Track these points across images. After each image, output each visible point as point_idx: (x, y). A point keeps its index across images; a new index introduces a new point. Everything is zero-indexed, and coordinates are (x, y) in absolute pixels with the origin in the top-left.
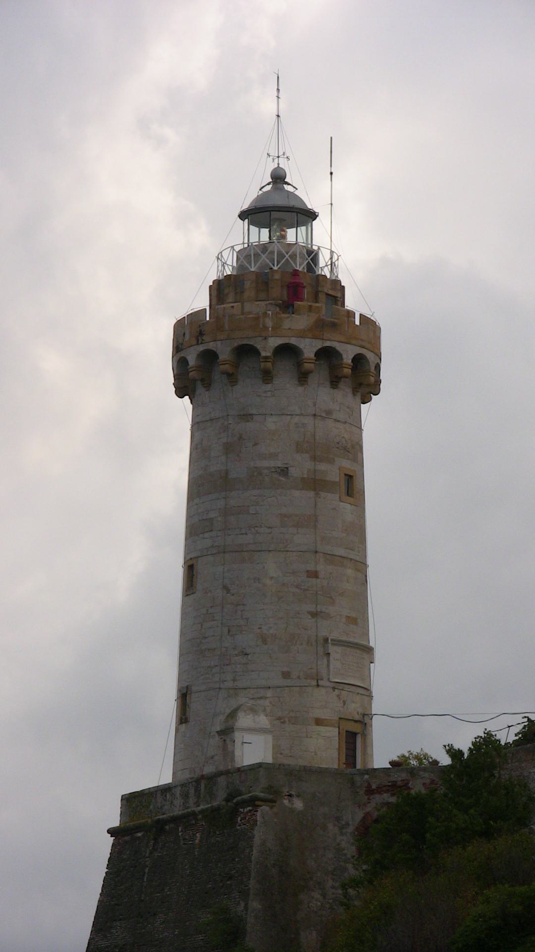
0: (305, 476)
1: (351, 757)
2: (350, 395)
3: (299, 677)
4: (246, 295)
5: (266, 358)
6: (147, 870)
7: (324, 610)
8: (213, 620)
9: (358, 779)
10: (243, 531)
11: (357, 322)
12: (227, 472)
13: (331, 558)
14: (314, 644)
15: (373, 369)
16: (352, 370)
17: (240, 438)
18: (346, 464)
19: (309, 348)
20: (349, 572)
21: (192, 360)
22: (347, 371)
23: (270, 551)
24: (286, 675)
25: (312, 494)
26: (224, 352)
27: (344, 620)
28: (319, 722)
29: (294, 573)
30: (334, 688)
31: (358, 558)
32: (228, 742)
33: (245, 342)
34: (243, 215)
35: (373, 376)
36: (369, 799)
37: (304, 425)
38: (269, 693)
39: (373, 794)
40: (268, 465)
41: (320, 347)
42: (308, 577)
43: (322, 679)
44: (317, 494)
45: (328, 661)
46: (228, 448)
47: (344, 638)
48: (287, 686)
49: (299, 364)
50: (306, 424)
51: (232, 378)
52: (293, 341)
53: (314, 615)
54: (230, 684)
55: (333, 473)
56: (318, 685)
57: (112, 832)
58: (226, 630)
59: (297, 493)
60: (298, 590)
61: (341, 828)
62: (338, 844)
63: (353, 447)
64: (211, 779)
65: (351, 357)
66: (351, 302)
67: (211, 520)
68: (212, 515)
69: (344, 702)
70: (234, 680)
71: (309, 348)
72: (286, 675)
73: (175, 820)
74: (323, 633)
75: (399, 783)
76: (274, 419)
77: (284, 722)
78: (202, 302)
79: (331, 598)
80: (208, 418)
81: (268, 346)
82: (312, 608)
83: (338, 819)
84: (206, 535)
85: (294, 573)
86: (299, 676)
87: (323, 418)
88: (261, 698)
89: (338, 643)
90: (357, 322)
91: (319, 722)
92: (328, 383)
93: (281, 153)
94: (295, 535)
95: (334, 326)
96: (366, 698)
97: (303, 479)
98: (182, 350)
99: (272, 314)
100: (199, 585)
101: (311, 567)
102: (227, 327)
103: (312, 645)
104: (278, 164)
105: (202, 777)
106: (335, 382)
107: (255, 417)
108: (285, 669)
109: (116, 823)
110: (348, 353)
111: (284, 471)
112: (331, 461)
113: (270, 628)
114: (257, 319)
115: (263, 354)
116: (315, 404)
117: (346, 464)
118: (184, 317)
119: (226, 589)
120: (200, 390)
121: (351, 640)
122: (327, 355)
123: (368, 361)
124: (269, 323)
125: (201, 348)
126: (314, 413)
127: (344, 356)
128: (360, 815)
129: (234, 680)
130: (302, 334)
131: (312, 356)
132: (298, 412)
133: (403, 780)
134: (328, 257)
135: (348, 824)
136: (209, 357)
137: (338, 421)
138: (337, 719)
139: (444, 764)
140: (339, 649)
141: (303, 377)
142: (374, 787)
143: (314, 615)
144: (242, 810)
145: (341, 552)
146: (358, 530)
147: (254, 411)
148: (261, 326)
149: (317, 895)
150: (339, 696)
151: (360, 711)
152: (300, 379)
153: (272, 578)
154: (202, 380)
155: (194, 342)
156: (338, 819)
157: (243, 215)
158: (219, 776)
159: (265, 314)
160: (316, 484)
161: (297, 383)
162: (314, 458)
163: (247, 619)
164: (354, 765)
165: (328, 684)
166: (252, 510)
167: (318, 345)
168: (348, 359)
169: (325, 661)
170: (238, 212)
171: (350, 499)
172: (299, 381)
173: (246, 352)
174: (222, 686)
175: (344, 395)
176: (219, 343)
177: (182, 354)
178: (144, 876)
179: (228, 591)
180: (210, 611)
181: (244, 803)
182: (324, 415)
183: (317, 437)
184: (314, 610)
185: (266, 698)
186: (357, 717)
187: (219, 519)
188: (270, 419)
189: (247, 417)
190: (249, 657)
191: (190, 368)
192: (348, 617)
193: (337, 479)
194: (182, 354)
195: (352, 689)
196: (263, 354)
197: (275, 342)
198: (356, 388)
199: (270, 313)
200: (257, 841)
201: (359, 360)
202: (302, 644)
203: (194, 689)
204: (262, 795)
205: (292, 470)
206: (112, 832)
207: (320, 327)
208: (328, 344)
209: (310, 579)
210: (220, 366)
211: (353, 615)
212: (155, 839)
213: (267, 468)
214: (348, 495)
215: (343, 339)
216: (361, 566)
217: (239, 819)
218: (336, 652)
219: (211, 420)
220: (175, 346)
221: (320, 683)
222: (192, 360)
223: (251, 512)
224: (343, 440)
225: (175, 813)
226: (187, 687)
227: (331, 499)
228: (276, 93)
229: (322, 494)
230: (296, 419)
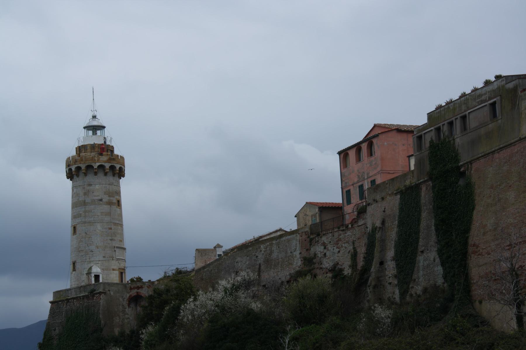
0: (107, 201)
1: (122, 281)
2: (118, 178)
3: (108, 258)
4: (88, 150)
5: (96, 168)
6: (64, 313)
8: (82, 242)
9: (128, 286)
10: (91, 217)
12: (85, 200)
13: (115, 224)
14: (111, 248)
17: (88, 191)
18: (117, 197)
19: (107, 165)
20: (120, 227)
21: (73, 169)
24: (104, 257)
25: (109, 206)
26: (83, 167)
27: (119, 241)
28: (113, 270)
29: (336, 239)
30: (117, 260)
31: (121, 224)
32: (89, 276)
33: (89, 164)
34: (85, 128)
36: (131, 291)
37: (106, 187)
38: (100, 262)
39: (132, 289)
40: (97, 198)
41: (110, 165)
42: (109, 229)
44: (111, 206)
45: (115, 252)
46: (85, 194)
47: (119, 246)
51: (85, 174)
52: (103, 164)
53: (111, 240)
54: (88, 260)
55: (115, 201)
56: (113, 260)
57: (51, 302)
58: (86, 245)
59: (105, 206)
61: (123, 299)
62: (123, 304)
63: (119, 192)
64: (84, 287)
65: (118, 167)
67: (81, 214)
68: (81, 213)
69: (120, 264)
70: (89, 259)
71: (107, 165)
72: (104, 257)
73: (73, 298)
74: (114, 245)
75: (140, 286)
76: (98, 185)
77: (104, 270)
78: (74, 153)
80: (78, 185)
81: (96, 166)
82: (110, 238)
83: (122, 297)
84: (79, 218)
85: (336, 239)
87: (111, 185)
88: (97, 264)
89: (117, 247)
91: (113, 270)
92: (112, 175)
93: (95, 110)
95: (114, 159)
96: (125, 262)
97: (106, 202)
98: (70, 166)
100: (78, 232)
101: (110, 227)
102: (84, 160)
105: (81, 286)
106: (114, 175)
107: (92, 185)
108: (104, 255)
109: (51, 299)
110: (118, 167)
111: (101, 200)
112: (113, 197)
114: (93, 158)
115: (95, 167)
116: (109, 181)
117: (117, 197)
118: (70, 157)
119: (86, 233)
120: (75, 177)
121: (121, 246)
122: (112, 168)
123: (122, 168)
124: (96, 159)
125: (76, 166)
126: (109, 183)
127: (117, 167)
128: (128, 295)
129: (89, 259)
130: (106, 162)
131: (108, 168)
132: (104, 183)
133: (141, 286)
134: (110, 139)
135: (125, 298)
136: (79, 169)
138: (118, 268)
139: (144, 281)
140: (118, 249)
141: (106, 174)
142: (132, 287)
143: (111, 240)
144: (96, 295)
145: (117, 222)
146: (121, 215)
147: (92, 183)
148: (94, 159)
149: (118, 318)
150: (118, 262)
151: (124, 266)
153: (99, 230)
154: (76, 175)
155: (74, 164)
156: (122, 297)
157: (85, 128)
158: (87, 286)
159: (95, 156)
160: (110, 203)
162: (109, 196)
163: (92, 242)
164: (122, 282)
165: (116, 259)
166: (93, 211)
167: (110, 164)
168: (118, 168)
170: (83, 127)
171: (119, 207)
173: (89, 167)
174: (86, 261)
175: (116, 178)
176: (82, 165)
177: (70, 167)
178: (63, 314)
179: (87, 234)
180: (81, 239)
181: (97, 294)
182: (111, 184)
183: (110, 190)
185: (99, 264)
186: (123, 268)
187: (83, 214)
189: (90, 185)
190: (94, 252)
192: (120, 240)
193: (116, 202)
194: (70, 167)
195: (122, 260)
196: (95, 167)
197: (98, 164)
200: (101, 304)
202: (108, 248)
203: (77, 261)
204: (102, 291)
205: (103, 200)
206: (51, 302)
207: (110, 160)
208: (112, 164)
209: (109, 230)
211: (121, 239)
212: (66, 304)
213: (97, 199)
214: (118, 206)
215: (116, 163)
216: (122, 225)
217: (95, 298)
218: (117, 250)
219: (79, 186)
220: (67, 165)
221: (113, 259)
222: (73, 169)
223: (93, 212)
225: (73, 297)
226: (75, 261)
227: (114, 207)
229: (112, 206)
230: (104, 185)
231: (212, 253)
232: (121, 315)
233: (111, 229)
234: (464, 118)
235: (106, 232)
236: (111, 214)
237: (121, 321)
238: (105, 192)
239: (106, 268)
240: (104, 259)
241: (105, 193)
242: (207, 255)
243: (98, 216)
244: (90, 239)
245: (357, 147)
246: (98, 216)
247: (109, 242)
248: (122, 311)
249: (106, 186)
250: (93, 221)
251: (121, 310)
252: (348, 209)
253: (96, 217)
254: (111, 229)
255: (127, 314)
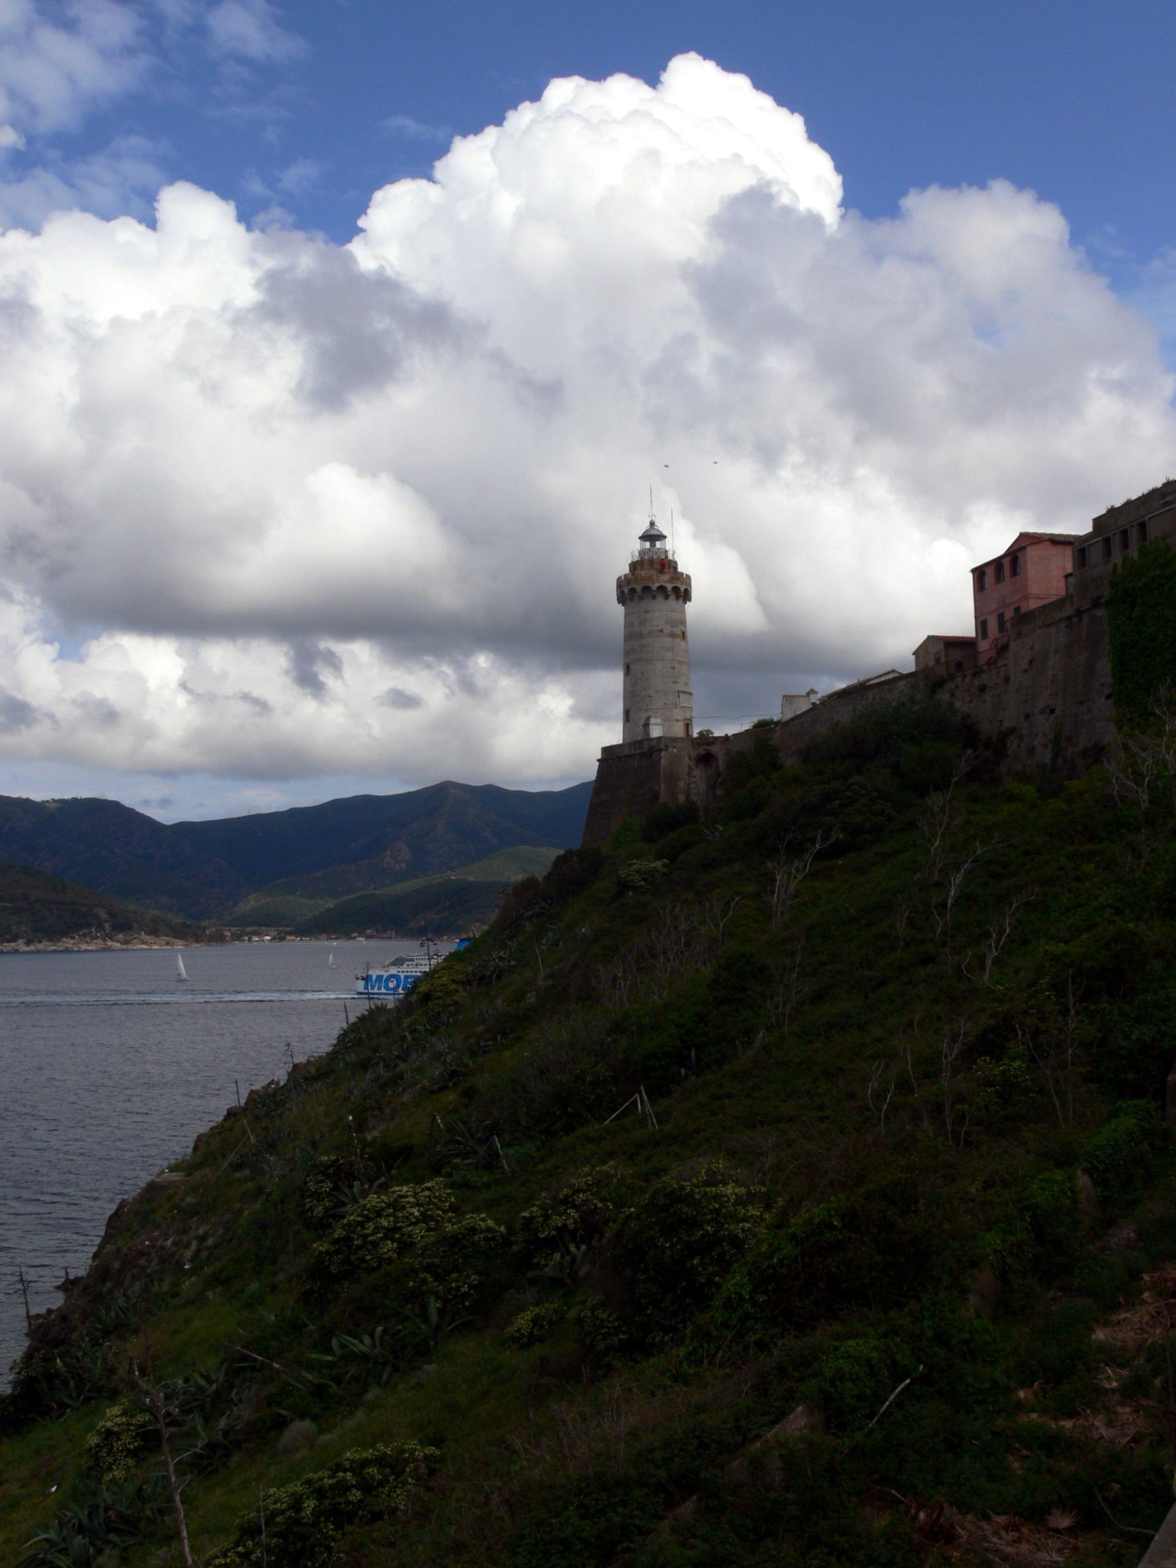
71: (669, 587)
81: (655, 587)
110: (682, 588)
167: (673, 585)
189: (648, 612)
197: (658, 585)
234: (1142, 526)
245: (997, 563)
252: (984, 646)
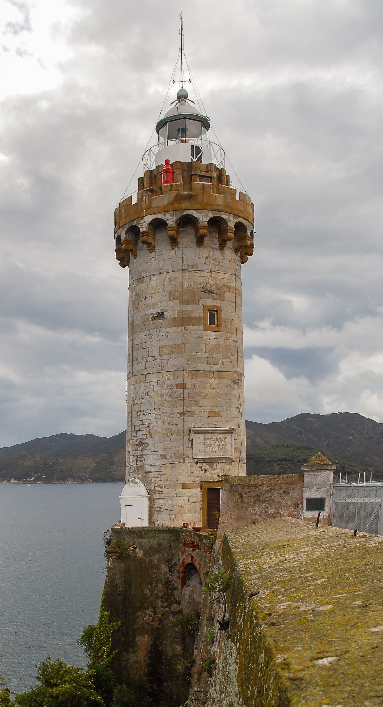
0: (176, 316)
5: (143, 233)
7: (189, 410)
11: (238, 198)
14: (182, 434)
15: (249, 233)
16: (234, 235)
22: (231, 235)
23: (153, 373)
24: (163, 457)
25: (180, 328)
28: (184, 486)
35: (249, 240)
37: (175, 279)
43: (188, 458)
48: (164, 464)
49: (197, 230)
50: (176, 277)
52: (160, 216)
53: (182, 414)
56: (184, 462)
59: (169, 330)
60: (170, 399)
66: (233, 184)
72: (163, 457)
76: (156, 277)
79: (195, 400)
82: (181, 410)
86: (171, 457)
87: (190, 271)
90: (238, 198)
91: (184, 486)
92: (195, 244)
94: (168, 360)
99: (146, 198)
101: (180, 382)
103: (180, 435)
104: (182, 87)
108: (162, 453)
111: (161, 315)
112: (196, 302)
113: (154, 426)
137: (203, 271)
143: (182, 414)
147: (145, 275)
149: (149, 612)
152: (199, 243)
161: (170, 248)
162: (182, 302)
165: (193, 460)
167: (210, 215)
168: (231, 225)
169: (190, 444)
172: (172, 246)
182: (190, 268)
184: (182, 411)
188: (153, 278)
191: (168, 228)
196: (141, 230)
197: (149, 219)
198: (222, 244)
199: (145, 197)
201: (239, 227)
202: (172, 435)
208: (217, 214)
210: (169, 232)
215: (197, 206)
218: (198, 439)
221: (186, 460)
224: (208, 284)
228: (178, 31)
230: (169, 276)
231: (286, 493)
232: (160, 604)
233: (183, 386)
235: (171, 396)
236: (184, 347)
237: (157, 619)
238: (170, 294)
239: (167, 482)
240: (164, 462)
241: (172, 296)
242: (264, 502)
243: (153, 357)
244: (139, 413)
246: (153, 357)
247: (177, 419)
248: (165, 594)
249: (175, 275)
250: (145, 372)
251: (161, 594)
253: (148, 359)
254: (183, 386)
255: (176, 603)
